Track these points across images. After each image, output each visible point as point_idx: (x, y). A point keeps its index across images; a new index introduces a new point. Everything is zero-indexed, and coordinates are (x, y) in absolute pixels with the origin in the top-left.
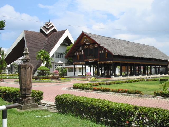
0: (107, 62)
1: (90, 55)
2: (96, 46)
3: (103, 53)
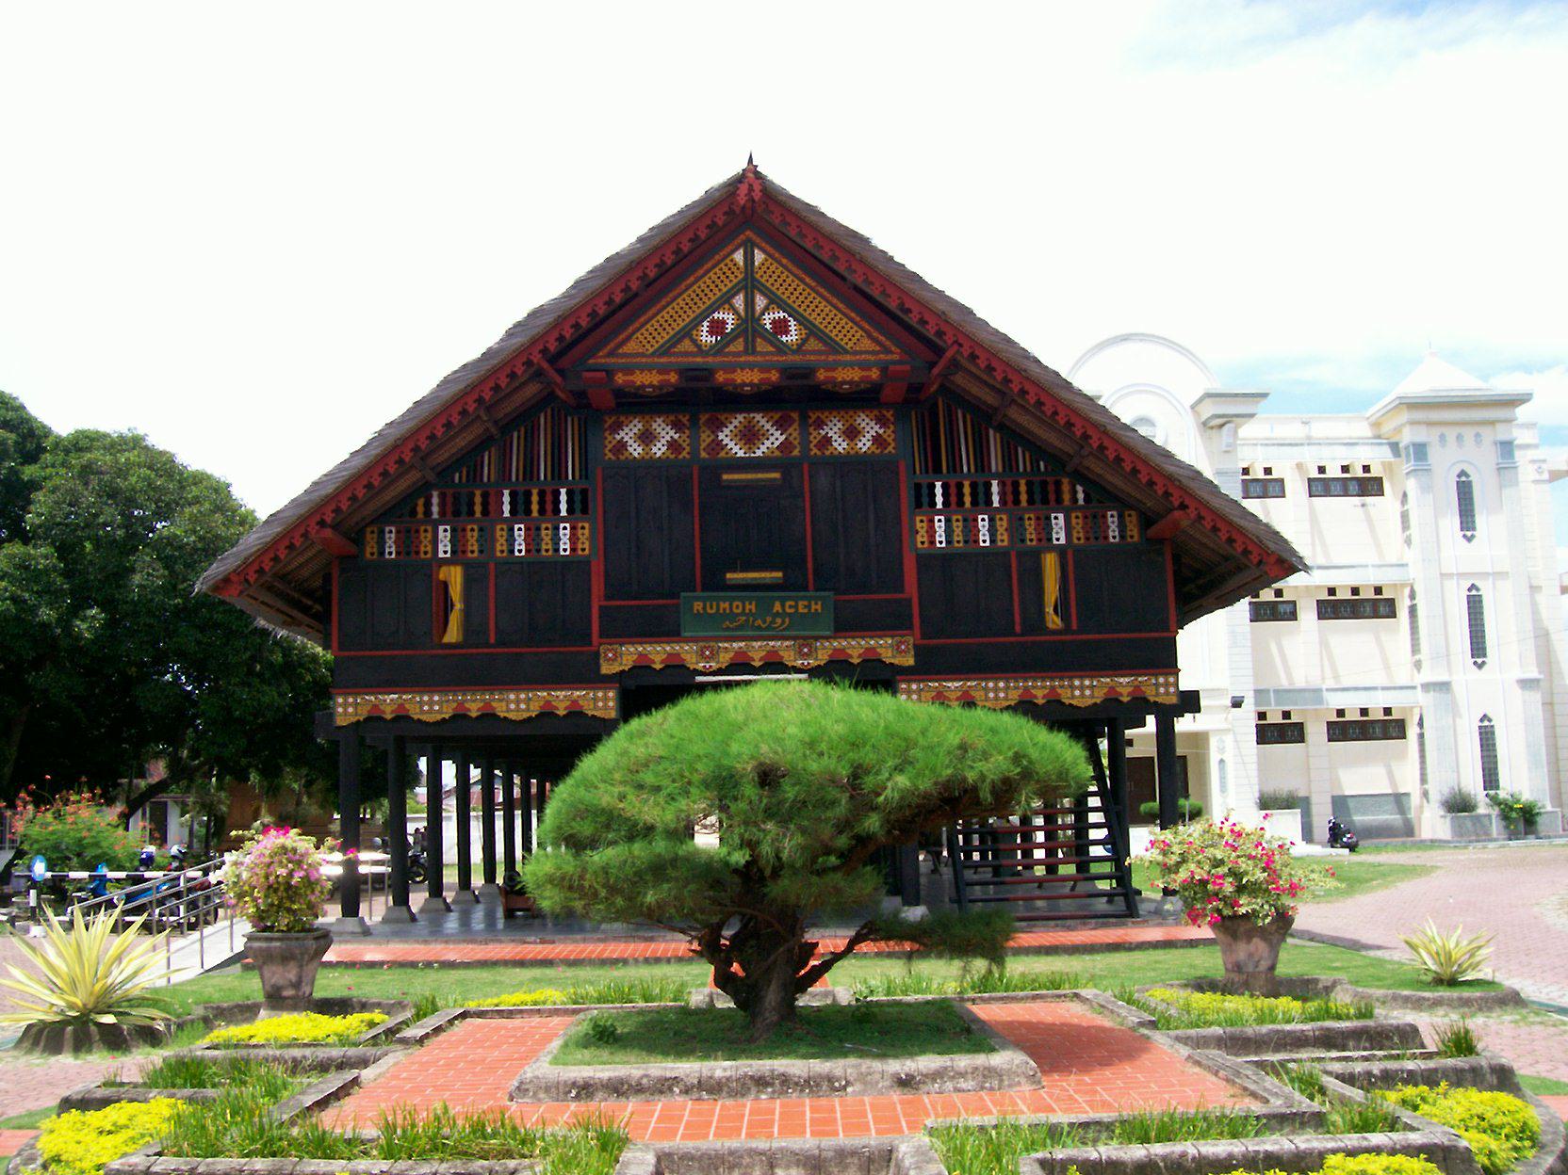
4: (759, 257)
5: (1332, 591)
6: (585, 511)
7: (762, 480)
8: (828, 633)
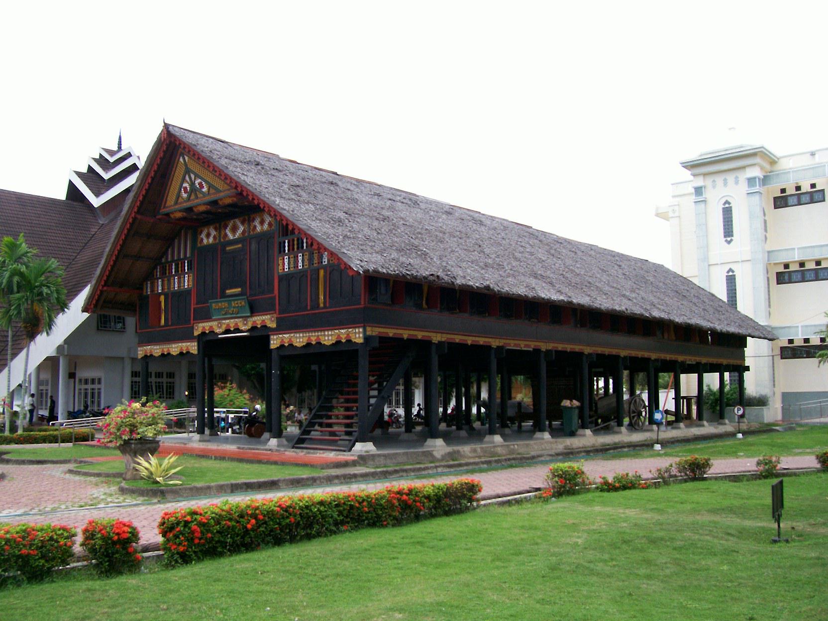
0: (328, 338)
1: (229, 292)
2: (262, 223)
3: (303, 273)
4: (186, 158)
5: (786, 266)
6: (191, 269)
7: (236, 248)
8: (249, 314)
